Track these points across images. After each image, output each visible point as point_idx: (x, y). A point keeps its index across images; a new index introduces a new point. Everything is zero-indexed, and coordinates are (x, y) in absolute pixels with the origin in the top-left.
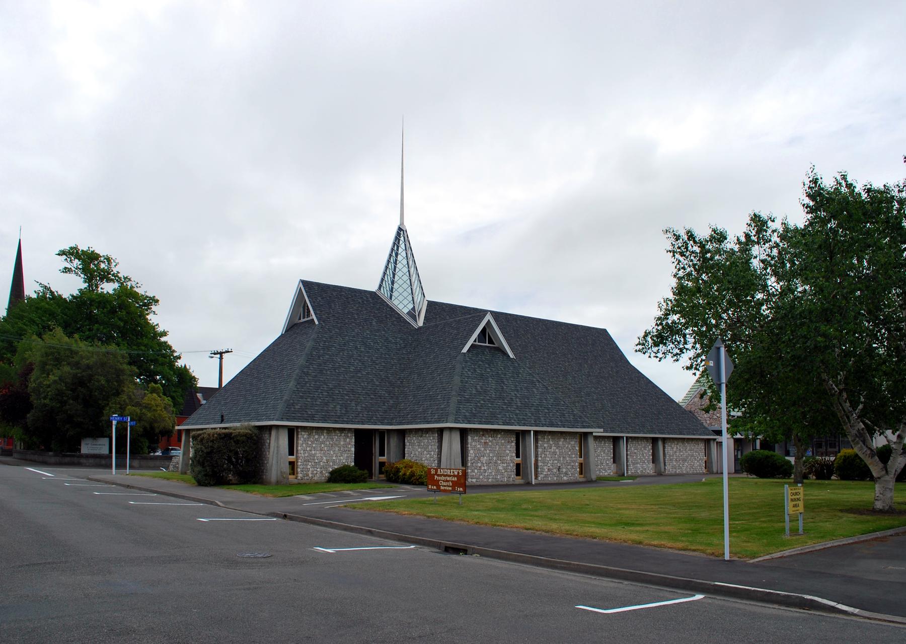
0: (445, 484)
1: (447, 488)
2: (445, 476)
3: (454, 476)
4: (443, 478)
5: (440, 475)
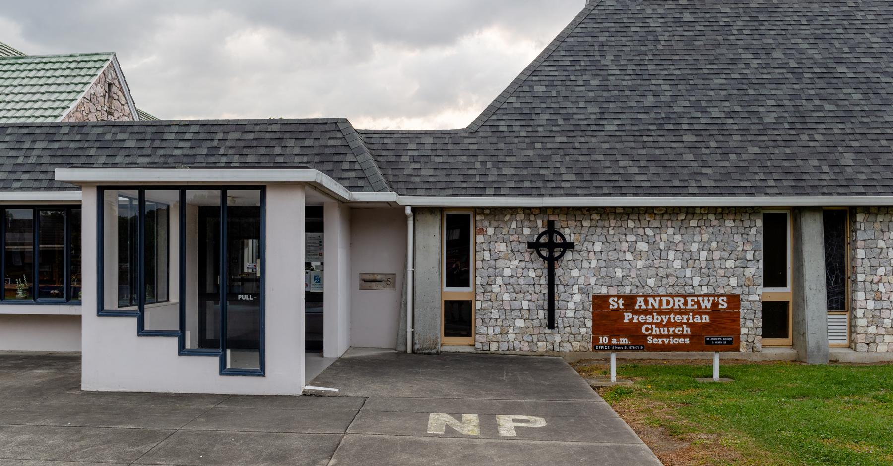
0: (656, 330)
1: (674, 341)
2: (661, 312)
3: (700, 311)
4: (657, 318)
5: (646, 312)
